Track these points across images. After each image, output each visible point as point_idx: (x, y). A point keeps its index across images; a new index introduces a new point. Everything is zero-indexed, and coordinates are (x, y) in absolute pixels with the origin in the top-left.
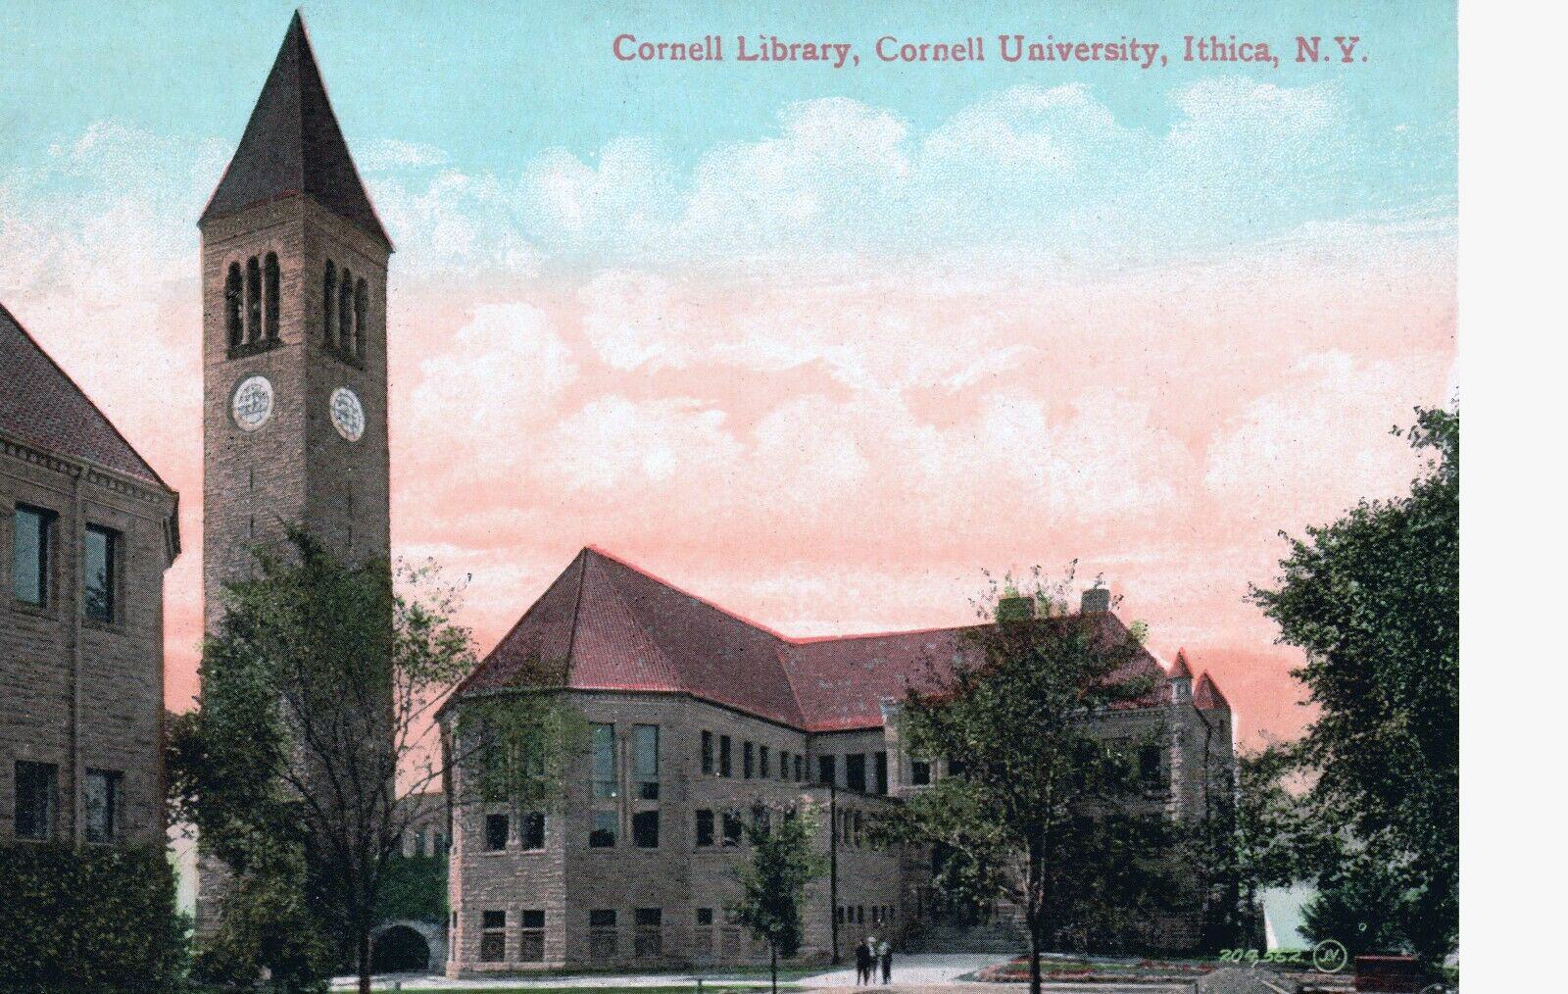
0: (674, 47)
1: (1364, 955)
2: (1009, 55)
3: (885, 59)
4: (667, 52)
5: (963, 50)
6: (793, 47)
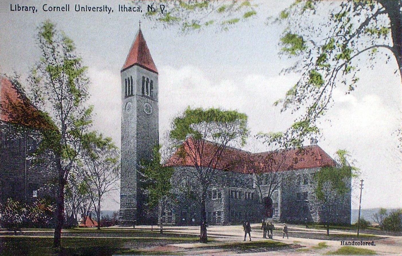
4: (56, 9)
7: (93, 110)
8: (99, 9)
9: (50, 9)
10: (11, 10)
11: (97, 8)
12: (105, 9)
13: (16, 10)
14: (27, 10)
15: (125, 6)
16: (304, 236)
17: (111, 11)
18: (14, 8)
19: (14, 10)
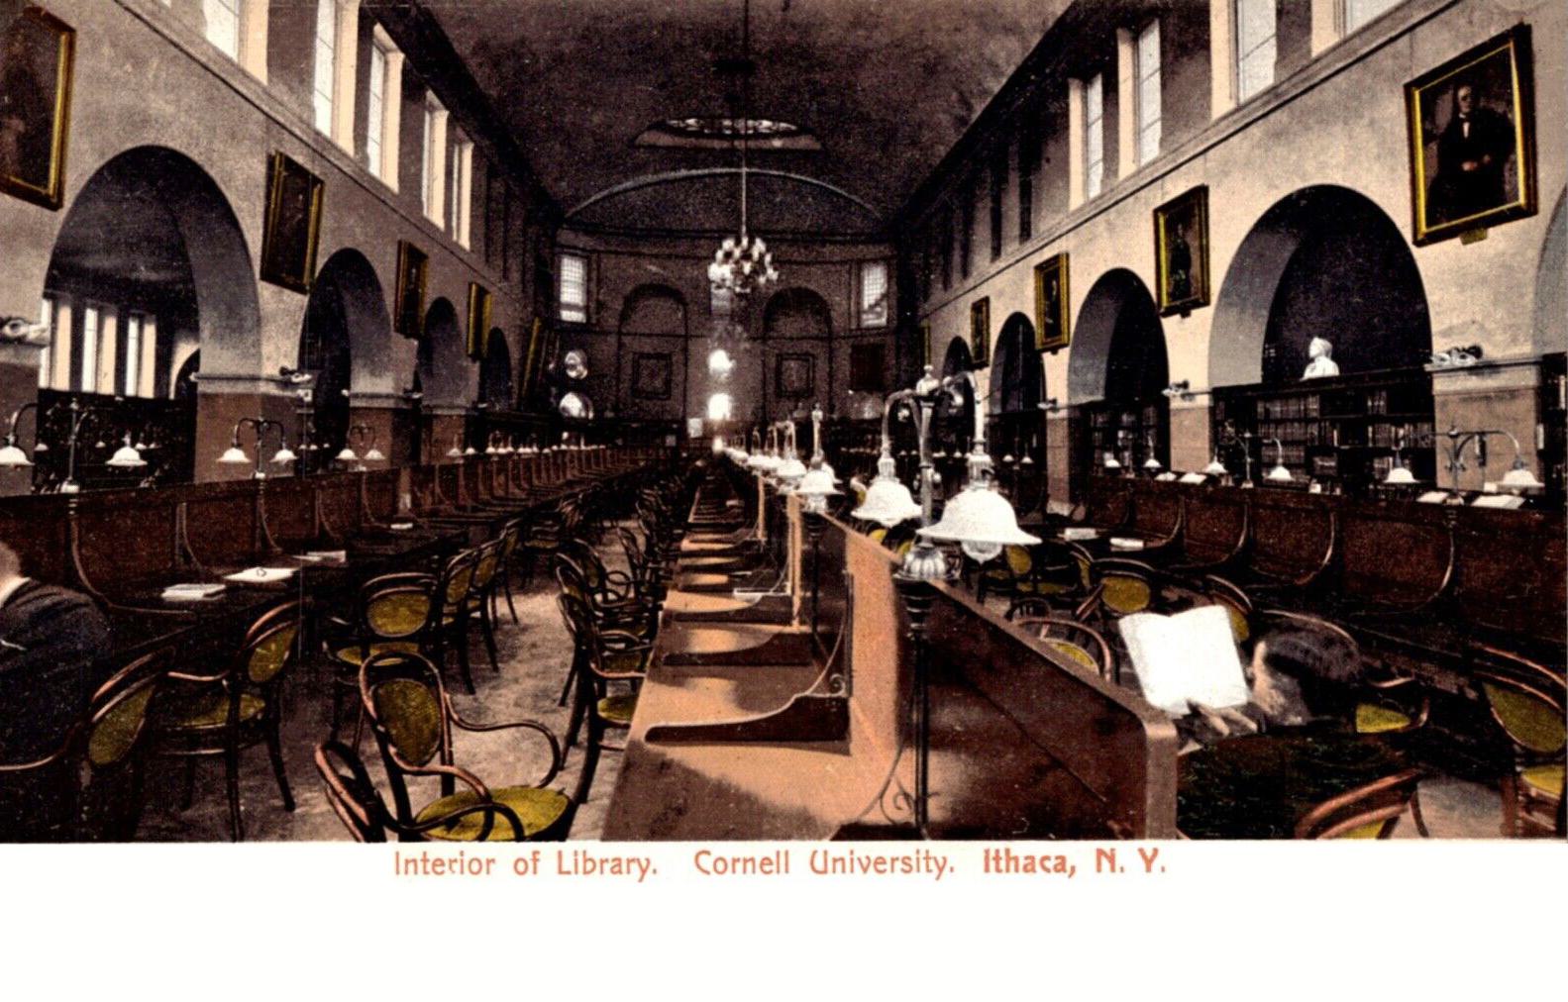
0: (746, 861)
1: (727, 174)
2: (565, 868)
3: (698, 866)
5: (771, 863)
6: (603, 862)
7: (524, 4)
8: (899, 865)
9: (720, 866)
10: (561, 872)
11: (893, 860)
12: (923, 863)
13: (576, 872)
14: (620, 872)
15: (589, 856)
16: (1119, 650)
17: (947, 870)
18: (568, 865)
19: (568, 873)
